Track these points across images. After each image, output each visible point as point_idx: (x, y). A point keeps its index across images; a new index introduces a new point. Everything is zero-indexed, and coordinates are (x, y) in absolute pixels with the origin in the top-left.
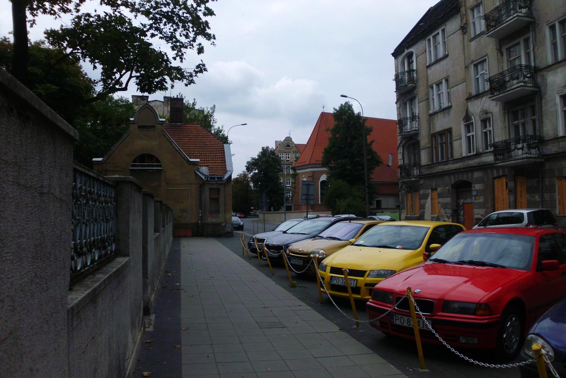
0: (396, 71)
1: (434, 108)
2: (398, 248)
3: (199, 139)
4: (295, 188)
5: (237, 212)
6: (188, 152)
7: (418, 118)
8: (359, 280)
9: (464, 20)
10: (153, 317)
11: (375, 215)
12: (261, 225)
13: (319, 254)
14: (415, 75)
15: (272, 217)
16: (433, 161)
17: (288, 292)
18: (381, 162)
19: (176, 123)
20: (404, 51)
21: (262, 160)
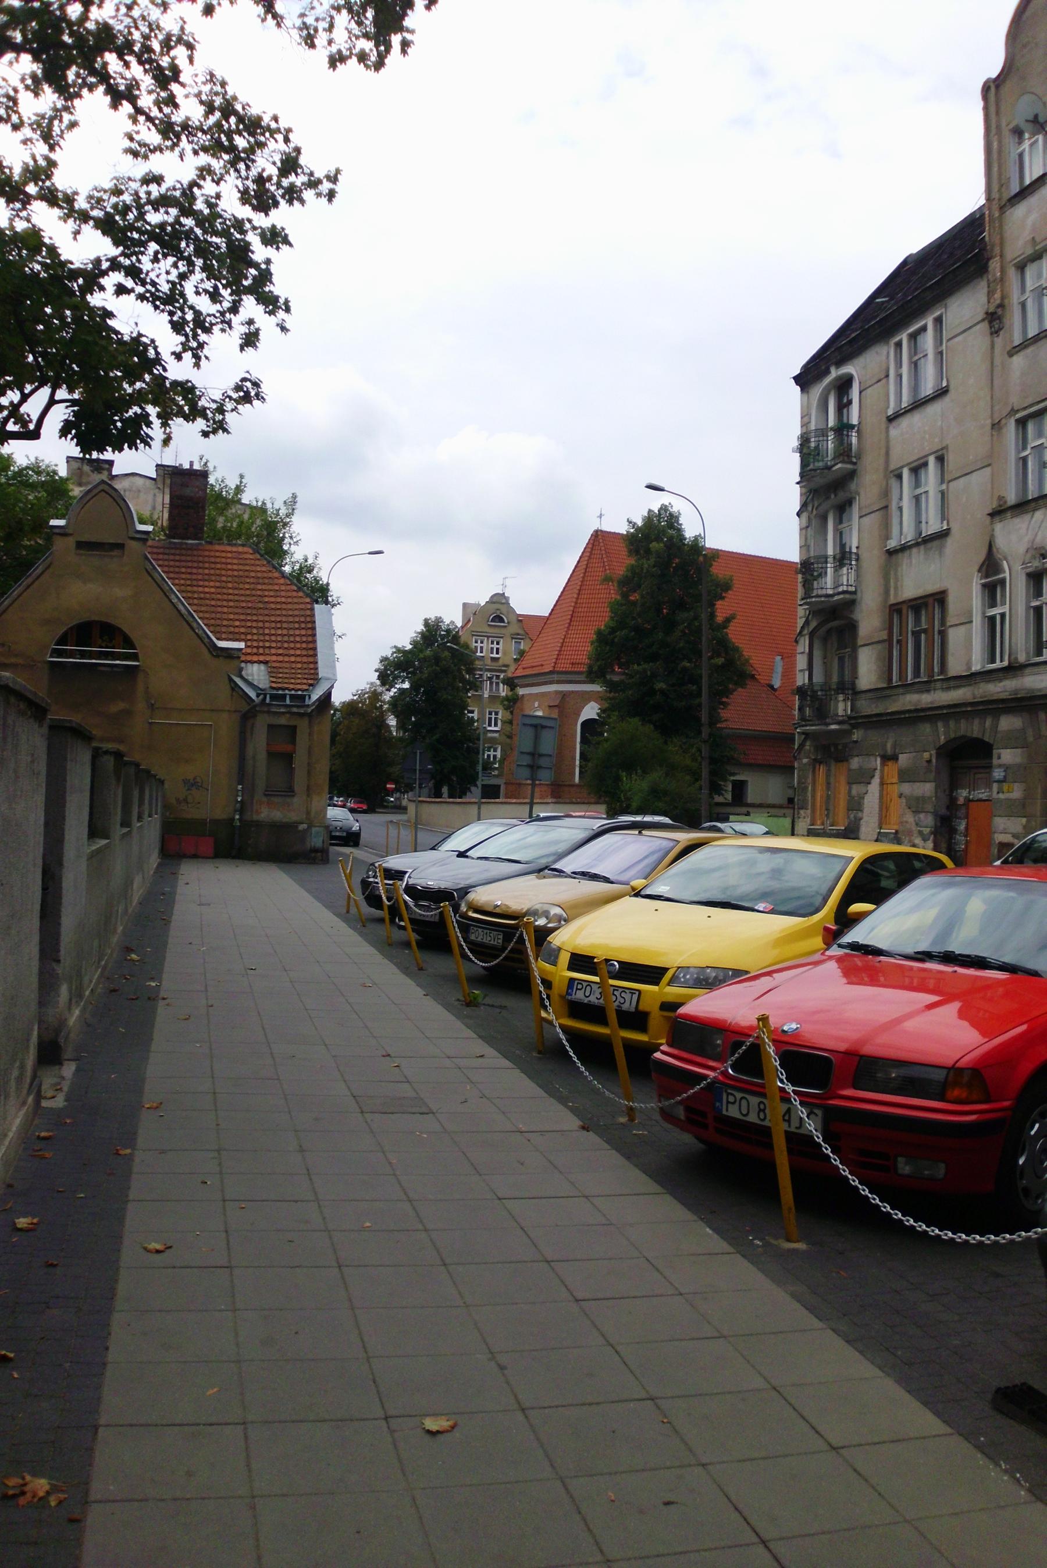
0: (804, 425)
1: (901, 534)
2: (761, 909)
3: (247, 586)
4: (510, 737)
5: (349, 796)
6: (212, 622)
7: (857, 560)
8: (647, 991)
9: (997, 295)
10: (69, 1070)
11: (726, 819)
12: (406, 835)
13: (547, 918)
14: (854, 440)
15: (438, 812)
16: (890, 680)
17: (454, 1018)
18: (753, 677)
19: (183, 538)
20: (827, 372)
21: (421, 656)
